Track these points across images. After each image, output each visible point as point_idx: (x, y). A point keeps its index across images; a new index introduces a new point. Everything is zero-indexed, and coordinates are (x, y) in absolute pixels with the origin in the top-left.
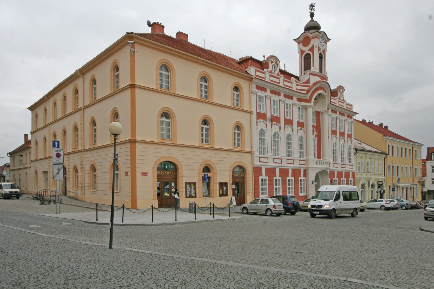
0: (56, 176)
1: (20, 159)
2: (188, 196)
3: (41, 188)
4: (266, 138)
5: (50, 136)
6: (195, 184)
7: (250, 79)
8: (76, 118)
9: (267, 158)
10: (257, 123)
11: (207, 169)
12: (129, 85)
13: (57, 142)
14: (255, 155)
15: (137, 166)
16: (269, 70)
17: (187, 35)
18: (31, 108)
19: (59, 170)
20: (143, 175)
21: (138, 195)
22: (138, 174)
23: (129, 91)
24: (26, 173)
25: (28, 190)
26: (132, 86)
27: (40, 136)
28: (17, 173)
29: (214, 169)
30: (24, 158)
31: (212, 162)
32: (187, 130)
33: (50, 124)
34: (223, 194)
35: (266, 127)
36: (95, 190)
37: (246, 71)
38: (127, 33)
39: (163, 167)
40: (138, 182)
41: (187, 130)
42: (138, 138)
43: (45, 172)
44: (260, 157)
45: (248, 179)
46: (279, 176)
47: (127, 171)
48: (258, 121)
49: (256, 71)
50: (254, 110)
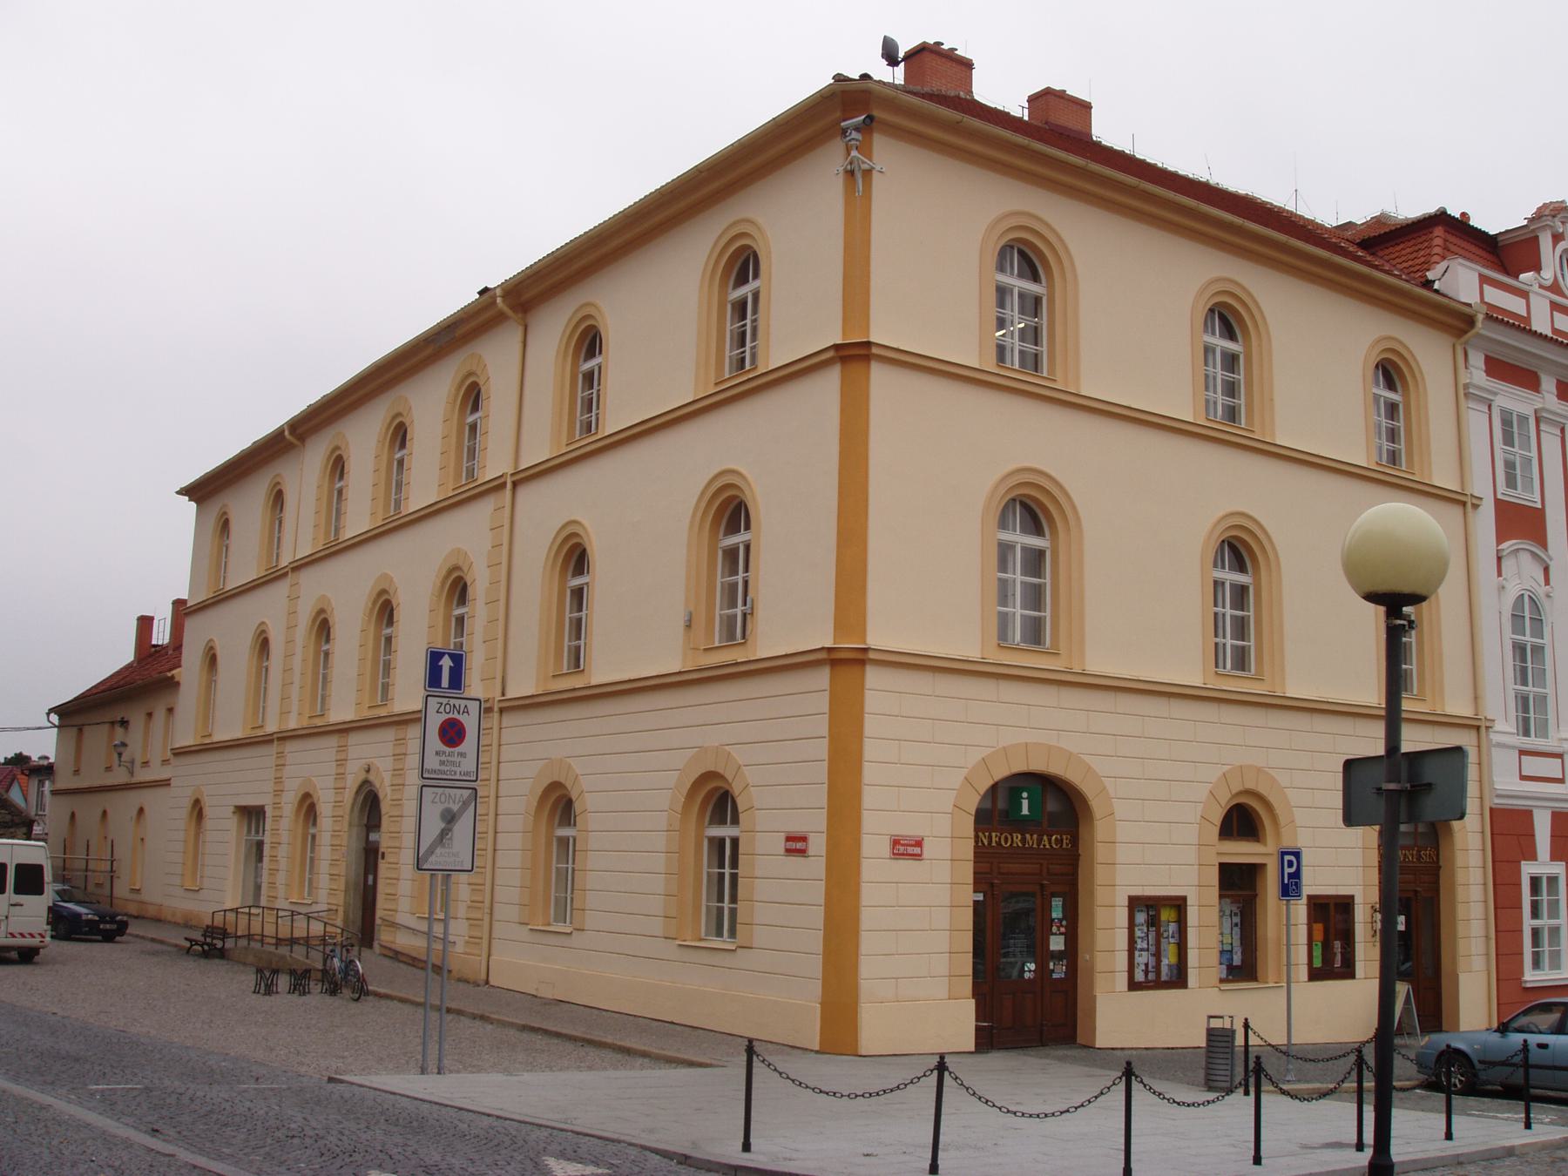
0: (431, 851)
1: (111, 736)
2: (1139, 976)
3: (221, 892)
4: (1546, 640)
5: (291, 627)
6: (1179, 904)
7: (1456, 322)
8: (467, 535)
9: (1560, 756)
10: (1499, 559)
11: (1241, 820)
12: (836, 347)
13: (452, 656)
14: (1495, 738)
15: (870, 798)
16: (1547, 274)
17: (1086, 107)
18: (200, 491)
19: (450, 818)
20: (897, 855)
21: (869, 969)
22: (874, 846)
23: (829, 384)
24: (141, 810)
25: (145, 896)
26: (854, 355)
27: (229, 631)
28: (89, 810)
29: (1282, 820)
30: (135, 736)
31: (1273, 780)
32: (1139, 601)
33: (299, 566)
34: (1333, 963)
35: (1547, 582)
36: (560, 927)
37: (1428, 284)
38: (839, 78)
39: (1001, 805)
40: (868, 894)
41: (1139, 601)
42: (878, 638)
43: (252, 815)
44: (1522, 752)
45: (1460, 877)
46: (1555, 857)
47: (796, 828)
48: (1504, 546)
49: (1484, 280)
50: (1481, 485)
